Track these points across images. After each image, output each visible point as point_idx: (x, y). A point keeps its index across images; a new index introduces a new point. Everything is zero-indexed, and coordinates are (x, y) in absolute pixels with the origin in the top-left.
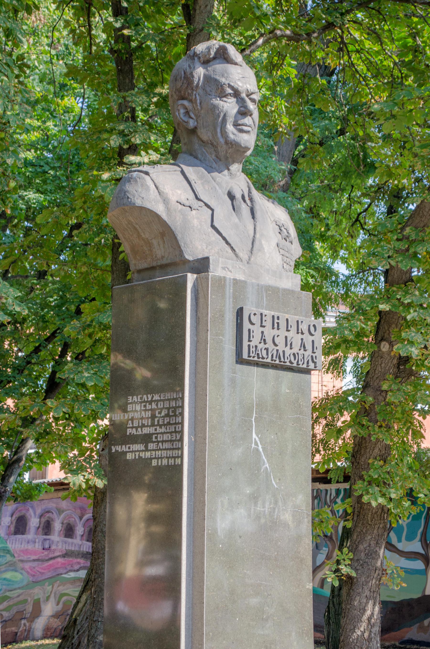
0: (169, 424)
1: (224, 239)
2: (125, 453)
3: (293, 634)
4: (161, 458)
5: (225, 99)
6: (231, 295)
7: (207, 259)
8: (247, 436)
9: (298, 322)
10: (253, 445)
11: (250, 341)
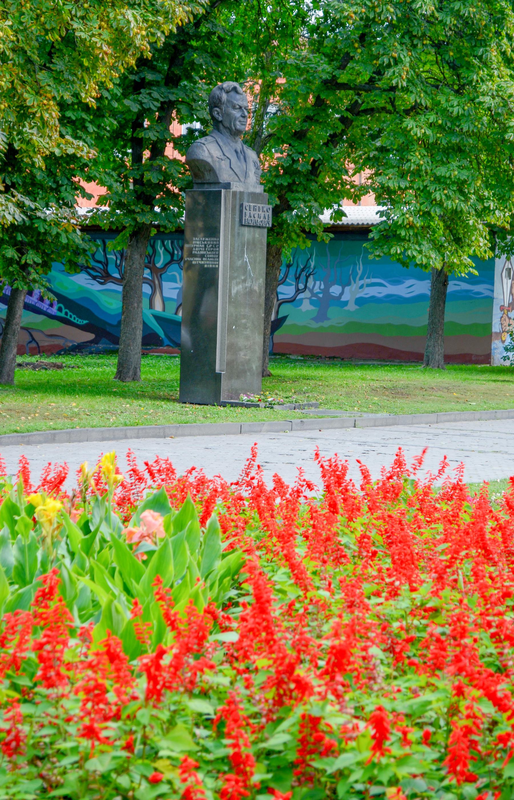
7: (229, 184)
8: (243, 256)
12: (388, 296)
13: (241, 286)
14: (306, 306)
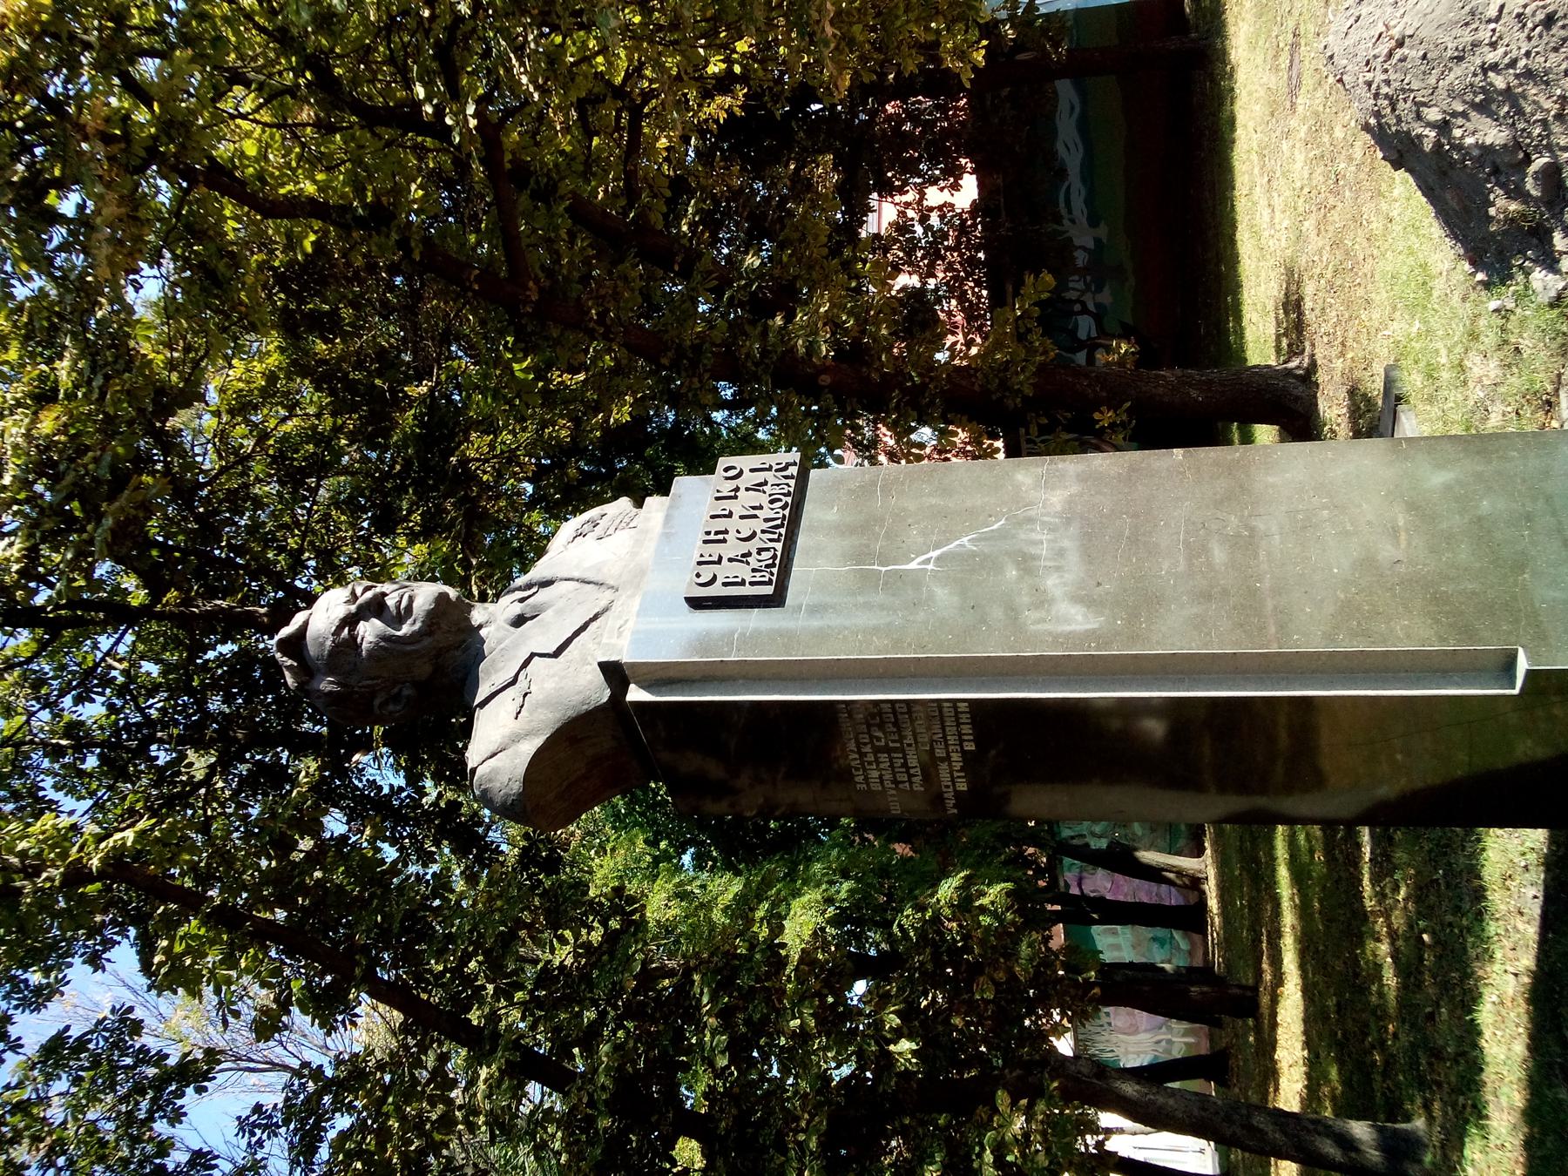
0: (896, 724)
1: (577, 633)
2: (957, 794)
3: (1270, 479)
4: (960, 735)
7: (604, 667)
8: (915, 580)
9: (717, 499)
10: (930, 567)
11: (743, 583)
12: (1084, 180)
13: (1051, 583)
14: (1105, 297)
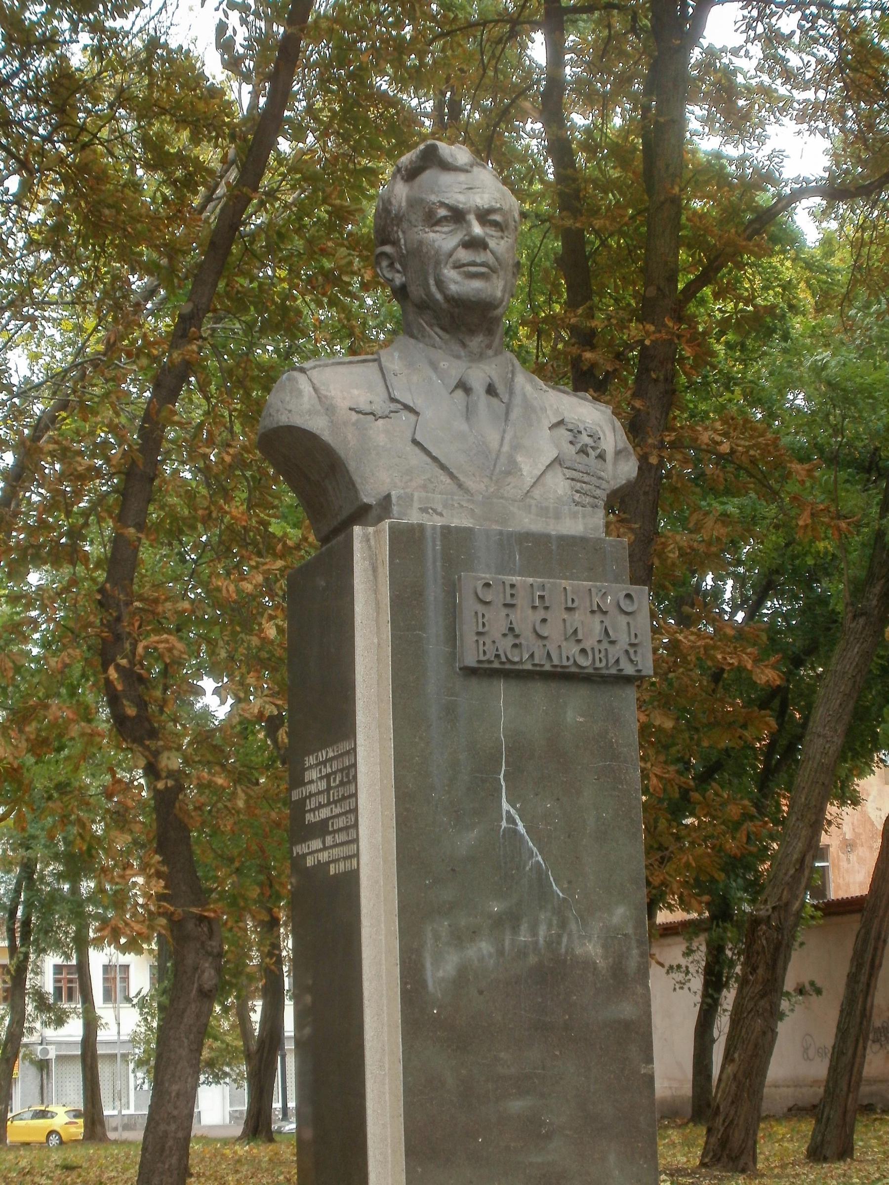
5: (437, 228)
6: (439, 556)
10: (504, 824)
